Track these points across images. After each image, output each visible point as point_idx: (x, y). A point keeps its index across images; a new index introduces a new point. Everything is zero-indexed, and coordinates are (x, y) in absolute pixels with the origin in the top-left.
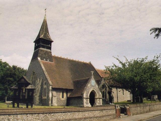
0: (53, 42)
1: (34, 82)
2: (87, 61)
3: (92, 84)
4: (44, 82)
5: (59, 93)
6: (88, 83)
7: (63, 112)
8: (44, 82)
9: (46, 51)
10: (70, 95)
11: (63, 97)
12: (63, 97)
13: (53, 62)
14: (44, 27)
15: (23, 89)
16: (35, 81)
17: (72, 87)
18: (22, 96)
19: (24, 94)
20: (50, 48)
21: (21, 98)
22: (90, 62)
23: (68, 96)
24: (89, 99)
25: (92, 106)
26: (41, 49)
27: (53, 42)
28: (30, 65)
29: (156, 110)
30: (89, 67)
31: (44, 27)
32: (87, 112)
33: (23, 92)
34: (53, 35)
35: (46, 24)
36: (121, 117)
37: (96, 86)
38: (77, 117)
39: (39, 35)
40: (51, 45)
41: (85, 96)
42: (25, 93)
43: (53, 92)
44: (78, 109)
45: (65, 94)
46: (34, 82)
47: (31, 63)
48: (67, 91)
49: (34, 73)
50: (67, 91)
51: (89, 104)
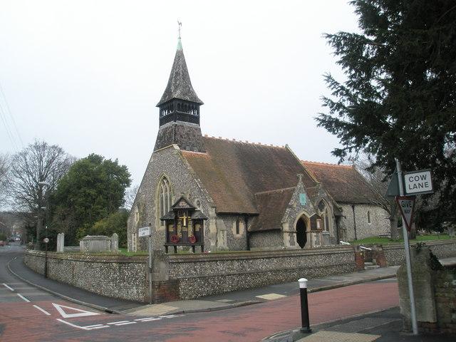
0: (201, 104)
1: (166, 199)
2: (279, 144)
3: (301, 202)
4: (196, 200)
5: (229, 223)
7: (266, 258)
8: (196, 200)
11: (238, 232)
12: (238, 232)
13: (205, 152)
14: (180, 73)
15: (183, 219)
16: (171, 200)
17: (251, 210)
18: (182, 232)
19: (185, 229)
20: (196, 120)
21: (179, 235)
22: (287, 145)
23: (249, 228)
24: (295, 235)
25: (302, 248)
27: (201, 104)
28: (152, 161)
29: (448, 257)
30: (285, 158)
31: (180, 73)
32: (303, 258)
33: (183, 226)
34: (200, 87)
35: (184, 66)
36: (366, 268)
37: (309, 205)
38: (288, 266)
39: (168, 92)
41: (286, 227)
42: (187, 226)
43: (218, 221)
44: (412, 255)
45: (242, 226)
46: (166, 199)
47: (154, 156)
48: (246, 217)
49: (165, 178)
50: (246, 217)
51: (297, 244)
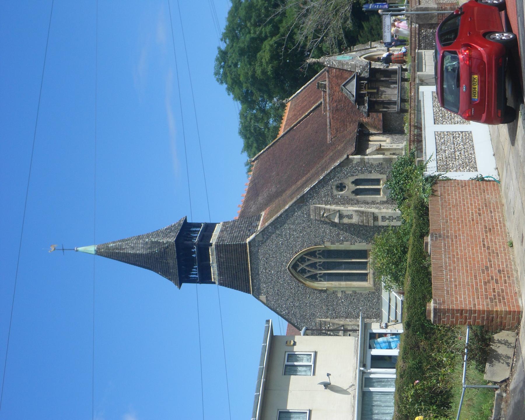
5: (370, 146)
6: (345, 67)
9: (222, 231)
10: (375, 128)
26: (214, 240)
40: (198, 225)
